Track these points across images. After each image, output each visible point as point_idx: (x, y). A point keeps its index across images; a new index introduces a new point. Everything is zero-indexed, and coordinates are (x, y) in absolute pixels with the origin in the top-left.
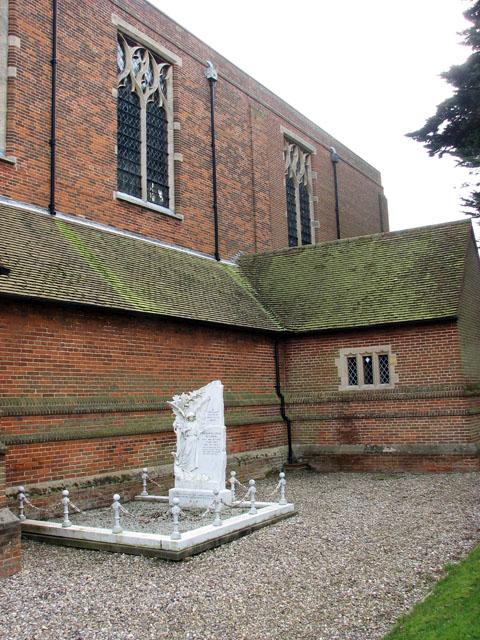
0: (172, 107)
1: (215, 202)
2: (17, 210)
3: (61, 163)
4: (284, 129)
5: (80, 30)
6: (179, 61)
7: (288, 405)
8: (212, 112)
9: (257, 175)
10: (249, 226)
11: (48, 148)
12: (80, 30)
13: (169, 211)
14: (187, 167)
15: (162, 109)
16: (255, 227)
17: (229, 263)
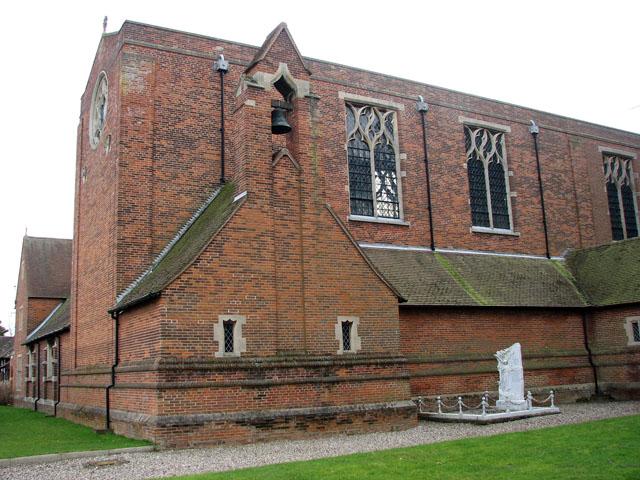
2: (413, 251)
3: (436, 217)
4: (602, 148)
5: (440, 135)
6: (508, 129)
7: (595, 355)
8: (537, 157)
11: (427, 212)
12: (440, 135)
14: (520, 200)
15: (500, 165)
17: (558, 259)
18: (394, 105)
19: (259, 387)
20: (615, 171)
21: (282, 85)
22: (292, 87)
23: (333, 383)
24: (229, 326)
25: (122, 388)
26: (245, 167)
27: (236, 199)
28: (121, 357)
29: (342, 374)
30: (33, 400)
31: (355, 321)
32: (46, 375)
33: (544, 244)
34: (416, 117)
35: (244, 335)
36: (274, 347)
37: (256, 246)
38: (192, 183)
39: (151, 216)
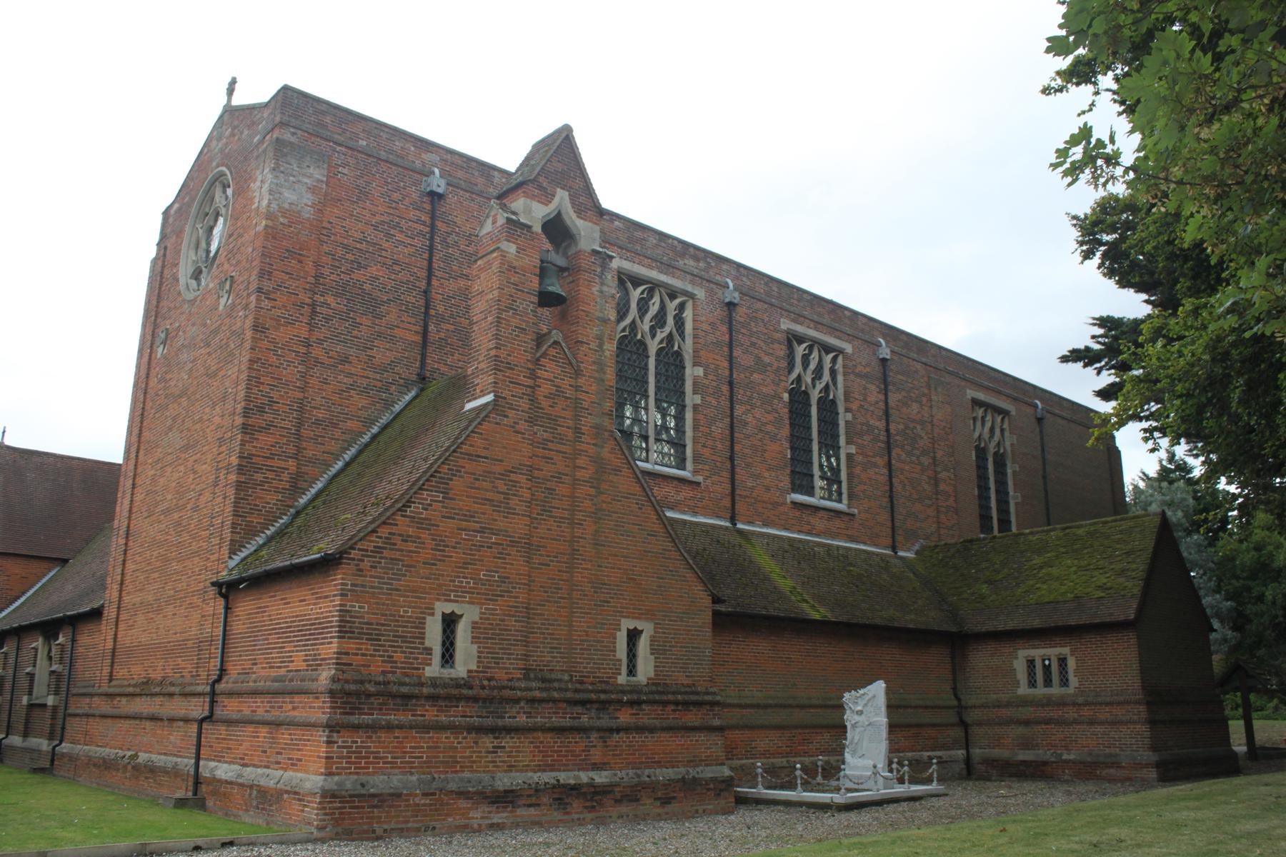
0: (842, 398)
1: (891, 491)
3: (741, 474)
4: (971, 393)
6: (848, 348)
7: (966, 708)
9: (939, 454)
10: (931, 512)
12: (753, 344)
13: (841, 507)
15: (833, 402)
16: (938, 512)
18: (689, 288)
19: (494, 731)
20: (987, 429)
21: (556, 230)
22: (575, 232)
23: (611, 730)
24: (450, 622)
25: (229, 722)
26: (493, 353)
27: (469, 406)
28: (229, 666)
29: (625, 717)
30: (44, 745)
31: (647, 628)
32: (30, 693)
33: (889, 531)
34: (720, 312)
35: (475, 640)
36: (521, 664)
37: (503, 488)
38: (371, 375)
39: (300, 424)
